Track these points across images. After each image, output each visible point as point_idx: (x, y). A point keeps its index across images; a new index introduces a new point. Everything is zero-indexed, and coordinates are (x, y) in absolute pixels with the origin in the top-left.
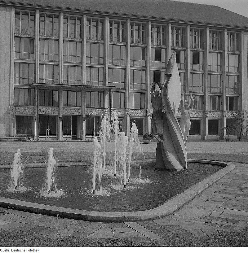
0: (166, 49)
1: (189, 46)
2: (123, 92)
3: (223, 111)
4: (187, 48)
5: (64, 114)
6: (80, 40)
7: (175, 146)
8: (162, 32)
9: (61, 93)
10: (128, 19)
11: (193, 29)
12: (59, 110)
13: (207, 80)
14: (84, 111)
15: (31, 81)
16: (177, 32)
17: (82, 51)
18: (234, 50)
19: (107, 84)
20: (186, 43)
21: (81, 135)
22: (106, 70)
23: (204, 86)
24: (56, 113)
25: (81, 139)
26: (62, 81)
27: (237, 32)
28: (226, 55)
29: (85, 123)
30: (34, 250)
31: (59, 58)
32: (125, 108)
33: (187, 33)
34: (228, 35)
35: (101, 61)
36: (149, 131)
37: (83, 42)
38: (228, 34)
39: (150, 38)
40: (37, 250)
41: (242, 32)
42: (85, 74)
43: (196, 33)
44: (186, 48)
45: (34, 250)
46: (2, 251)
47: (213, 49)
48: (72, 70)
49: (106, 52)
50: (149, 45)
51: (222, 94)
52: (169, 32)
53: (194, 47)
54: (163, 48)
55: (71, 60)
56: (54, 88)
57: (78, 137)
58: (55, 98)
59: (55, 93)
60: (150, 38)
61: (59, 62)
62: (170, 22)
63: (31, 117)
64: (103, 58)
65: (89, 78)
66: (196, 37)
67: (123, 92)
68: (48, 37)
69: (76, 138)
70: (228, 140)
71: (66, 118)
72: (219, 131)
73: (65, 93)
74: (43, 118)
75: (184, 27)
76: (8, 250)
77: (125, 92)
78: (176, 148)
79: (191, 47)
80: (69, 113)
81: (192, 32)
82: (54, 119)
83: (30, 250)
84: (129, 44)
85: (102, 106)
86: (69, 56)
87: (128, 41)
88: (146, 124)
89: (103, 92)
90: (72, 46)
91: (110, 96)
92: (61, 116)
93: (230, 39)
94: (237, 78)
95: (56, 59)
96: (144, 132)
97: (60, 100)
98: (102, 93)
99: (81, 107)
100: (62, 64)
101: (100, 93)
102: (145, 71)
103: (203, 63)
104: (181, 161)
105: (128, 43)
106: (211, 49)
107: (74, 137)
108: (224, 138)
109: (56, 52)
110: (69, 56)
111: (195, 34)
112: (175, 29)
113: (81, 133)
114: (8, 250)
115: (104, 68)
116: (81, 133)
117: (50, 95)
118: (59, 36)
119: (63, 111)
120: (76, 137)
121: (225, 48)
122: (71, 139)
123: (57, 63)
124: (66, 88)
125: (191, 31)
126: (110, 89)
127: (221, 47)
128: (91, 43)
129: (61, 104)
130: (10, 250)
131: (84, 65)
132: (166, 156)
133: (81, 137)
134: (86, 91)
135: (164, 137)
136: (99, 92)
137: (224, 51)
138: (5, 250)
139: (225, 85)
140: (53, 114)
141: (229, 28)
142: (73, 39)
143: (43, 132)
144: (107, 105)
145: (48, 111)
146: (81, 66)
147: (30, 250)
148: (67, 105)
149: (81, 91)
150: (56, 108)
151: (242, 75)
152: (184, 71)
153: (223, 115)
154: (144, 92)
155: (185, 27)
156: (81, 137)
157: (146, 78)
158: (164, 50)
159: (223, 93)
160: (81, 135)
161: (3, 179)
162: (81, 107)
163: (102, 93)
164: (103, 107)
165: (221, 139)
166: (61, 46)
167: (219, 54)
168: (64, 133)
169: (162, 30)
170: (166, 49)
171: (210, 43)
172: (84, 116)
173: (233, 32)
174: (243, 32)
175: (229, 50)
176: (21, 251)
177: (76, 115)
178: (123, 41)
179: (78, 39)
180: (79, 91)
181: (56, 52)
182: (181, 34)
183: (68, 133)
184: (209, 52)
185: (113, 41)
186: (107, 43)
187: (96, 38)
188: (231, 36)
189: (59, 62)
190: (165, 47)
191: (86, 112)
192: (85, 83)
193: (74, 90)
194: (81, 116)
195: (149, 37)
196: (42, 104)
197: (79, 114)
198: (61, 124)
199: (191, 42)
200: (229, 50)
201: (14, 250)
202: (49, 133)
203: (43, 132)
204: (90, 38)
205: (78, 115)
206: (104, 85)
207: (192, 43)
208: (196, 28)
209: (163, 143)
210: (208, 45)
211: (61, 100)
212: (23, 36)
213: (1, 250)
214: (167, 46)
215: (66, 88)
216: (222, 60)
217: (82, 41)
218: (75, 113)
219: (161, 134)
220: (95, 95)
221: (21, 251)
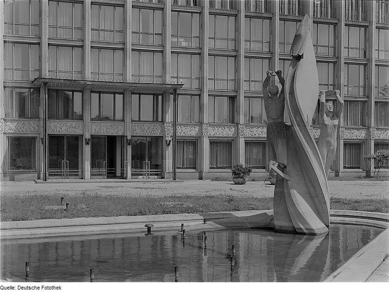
0: (236, 16)
1: (374, 19)
3: (369, 128)
5: (93, 133)
9: (87, 96)
13: (342, 73)
15: (32, 76)
18: (358, 19)
20: (368, 15)
21: (122, 170)
24: (78, 132)
25: (123, 177)
28: (344, 29)
29: (129, 149)
32: (201, 123)
35: (158, 40)
36: (242, 161)
37: (165, 9)
46: (3, 289)
47: (352, 19)
57: (118, 174)
58: (77, 109)
59: (78, 97)
63: (34, 138)
69: (115, 177)
71: (95, 140)
72: (363, 163)
73: (95, 96)
74: (56, 141)
76: (13, 288)
77: (200, 95)
79: (314, 15)
80: (102, 131)
82: (74, 142)
83: (47, 288)
85: (160, 120)
86: (101, 30)
91: (175, 100)
96: (234, 164)
98: (160, 97)
99: (123, 120)
101: (155, 96)
107: (112, 174)
108: (372, 174)
110: (101, 30)
114: (13, 288)
115: (162, 52)
117: (68, 102)
119: (90, 129)
120: (115, 173)
121: (374, 18)
122: (106, 177)
124: (97, 88)
126: (175, 90)
128: (215, 14)
129: (87, 117)
130: (16, 288)
131: (128, 47)
133: (122, 174)
134: (132, 93)
136: (154, 94)
137: (340, 20)
138: (8, 287)
139: (374, 83)
143: (54, 164)
145: (64, 128)
146: (123, 49)
147: (47, 288)
148: (100, 118)
149: (123, 93)
150: (80, 123)
153: (368, 134)
156: (122, 174)
159: (369, 97)
160: (122, 170)
161: (65, 61)
162: (123, 120)
163: (160, 97)
164: (162, 121)
165: (368, 176)
166: (87, 14)
167: (332, 27)
168: (92, 167)
171: (347, 8)
176: (33, 288)
180: (120, 93)
183: (99, 167)
184: (346, 25)
191: (130, 130)
192: (130, 79)
196: (52, 116)
197: (120, 134)
198: (87, 150)
201: (22, 288)
203: (54, 164)
207: (316, 10)
210: (374, 14)
211: (87, 107)
212: (320, 20)
213: (2, 288)
215: (97, 88)
216: (337, 36)
217: (124, 5)
218: (112, 132)
220: (147, 100)
221: (33, 288)
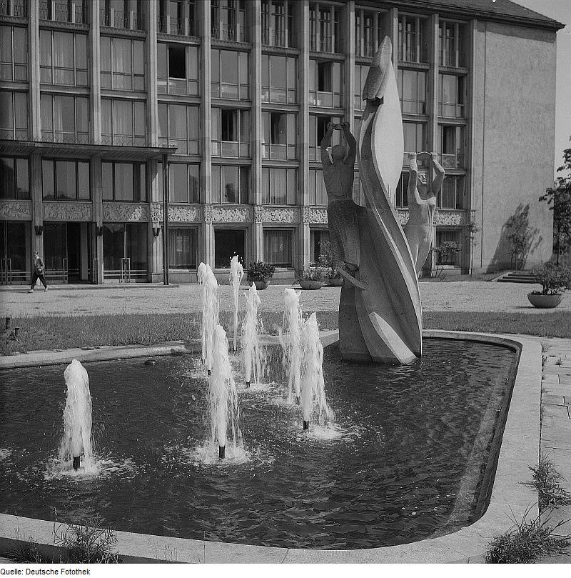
0: (342, 62)
2: (195, 163)
4: (347, 56)
5: (47, 218)
6: (23, 22)
7: (393, 297)
8: (287, 16)
10: (473, 19)
11: (402, 16)
12: (32, 209)
14: (97, 210)
16: (277, 10)
17: (90, 56)
19: (156, 141)
22: (152, 106)
23: (252, 142)
24: (25, 216)
25: (91, 280)
26: (38, 134)
27: (460, 21)
29: (100, 242)
30: (78, 572)
31: (29, 74)
33: (302, 15)
34: (400, 24)
37: (29, 25)
38: (399, 21)
39: (258, 29)
40: (84, 571)
41: (472, 21)
42: (98, 116)
43: (325, 14)
44: (346, 56)
45: (78, 572)
46: (4, 574)
47: (365, 54)
48: (180, 112)
49: (152, 61)
50: (257, 45)
51: (428, 168)
52: (305, 15)
53: (318, 50)
54: (337, 61)
55: (60, 78)
56: (18, 151)
57: (85, 276)
60: (258, 29)
61: (28, 83)
62: (437, 11)
64: (143, 76)
65: (106, 128)
66: (325, 23)
67: (195, 163)
68: (60, 23)
70: (442, 278)
71: (50, 229)
73: (107, 167)
75: (463, 22)
76: (19, 572)
78: (397, 303)
81: (358, 18)
82: (139, 232)
83: (70, 572)
84: (208, 43)
85: (143, 198)
87: (206, 34)
88: (253, 241)
89: (146, 163)
90: (120, 47)
92: (38, 222)
93: (405, 31)
94: (424, 128)
95: (82, 80)
97: (36, 181)
98: (143, 167)
99: (90, 200)
100: (97, 93)
101: (136, 165)
102: (296, 113)
103: (248, 82)
104: (408, 336)
105: (206, 38)
106: (360, 55)
108: (433, 273)
109: (82, 64)
111: (365, 23)
112: (318, 10)
113: (90, 266)
114: (19, 572)
116: (90, 266)
118: (27, 14)
120: (79, 276)
123: (24, 87)
125: (357, 15)
126: (165, 156)
127: (426, 57)
129: (37, 194)
130: (24, 572)
132: (371, 326)
134: (103, 161)
135: (363, 271)
138: (12, 571)
140: (17, 218)
141: (445, 12)
142: (64, 24)
144: (156, 196)
150: (26, 203)
151: (473, 124)
152: (341, 113)
154: (247, 162)
155: (386, 11)
156: (90, 276)
157: (201, 125)
158: (294, 59)
163: (143, 167)
164: (146, 201)
169: (287, 11)
170: (342, 62)
172: (99, 225)
173: (370, 8)
174: (475, 22)
175: (404, 60)
176: (48, 572)
177: (79, 220)
178: (191, 33)
179: (76, 25)
180: (25, 158)
181: (82, 64)
182: (333, 21)
185: (221, 39)
186: (152, 37)
187: (123, 24)
188: (409, 25)
189: (28, 83)
190: (249, 47)
192: (98, 139)
193: (72, 156)
194: (90, 224)
195: (257, 26)
197: (87, 219)
198: (39, 242)
199: (356, 43)
200: (404, 60)
201: (33, 572)
202: (9, 268)
204: (108, 23)
205: (82, 220)
206: (30, 139)
208: (450, 20)
209: (360, 290)
213: (3, 571)
214: (301, 50)
216: (429, 89)
219: (356, 266)
220: (125, 171)
221: (48, 572)
